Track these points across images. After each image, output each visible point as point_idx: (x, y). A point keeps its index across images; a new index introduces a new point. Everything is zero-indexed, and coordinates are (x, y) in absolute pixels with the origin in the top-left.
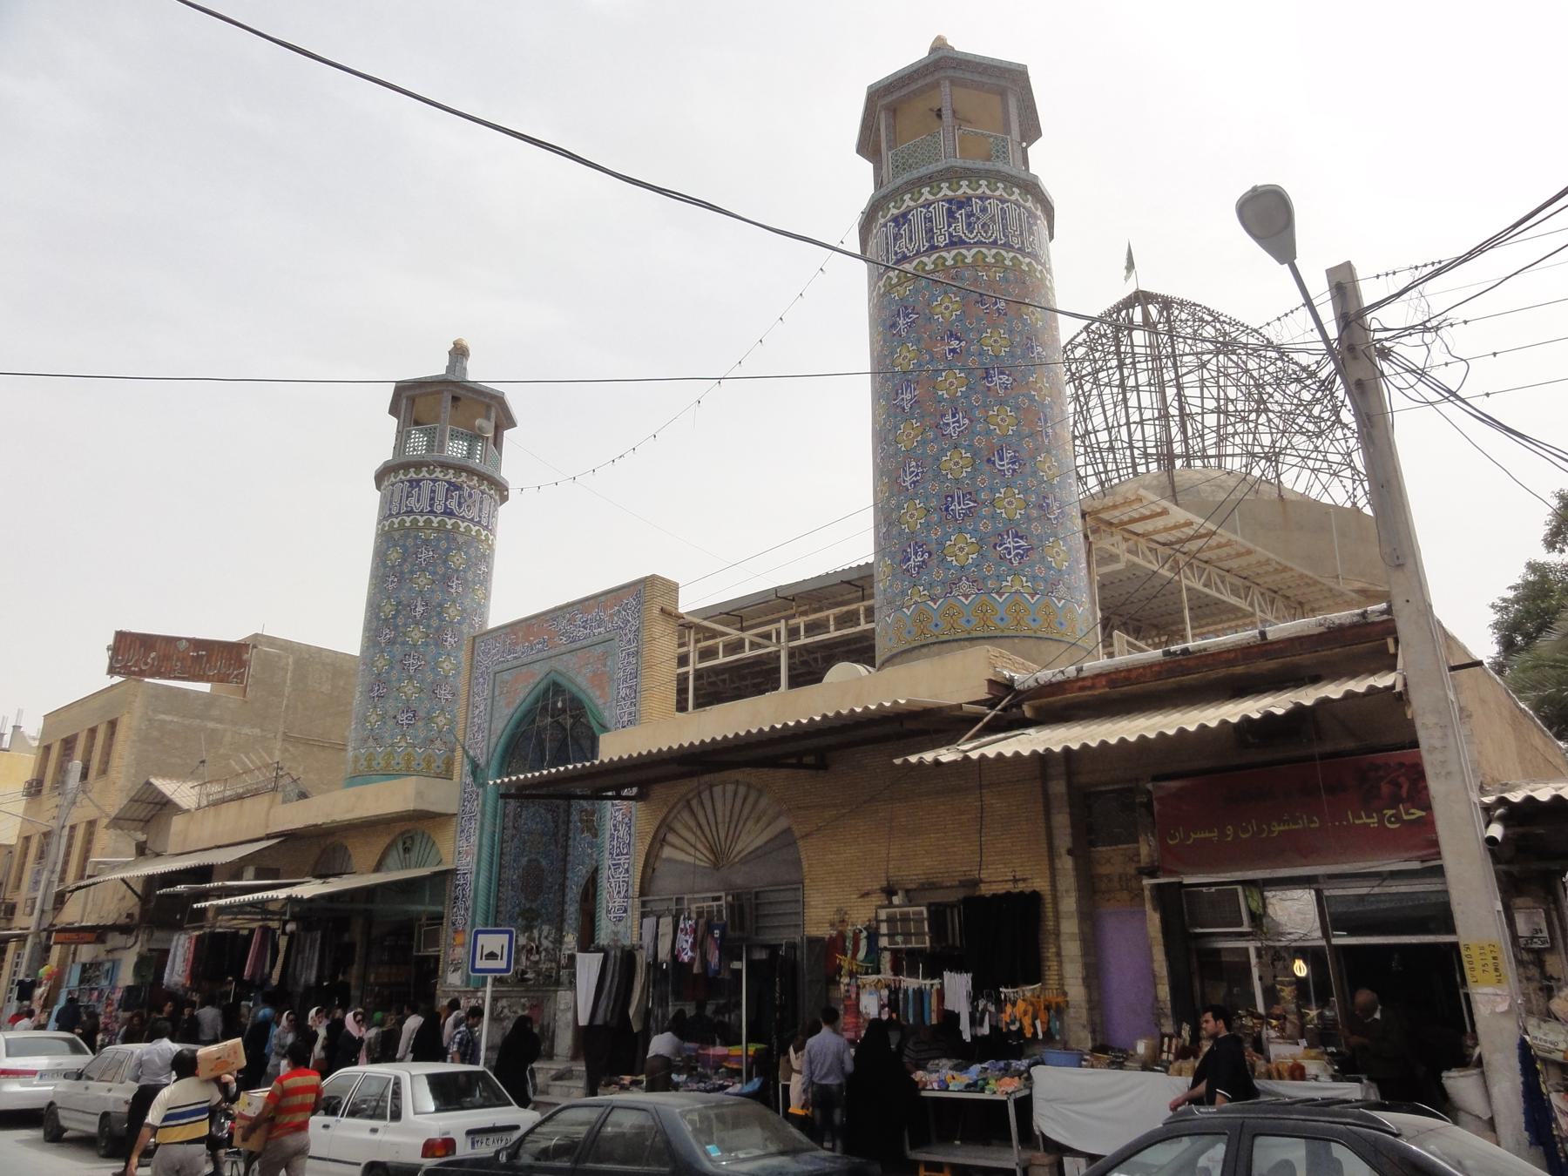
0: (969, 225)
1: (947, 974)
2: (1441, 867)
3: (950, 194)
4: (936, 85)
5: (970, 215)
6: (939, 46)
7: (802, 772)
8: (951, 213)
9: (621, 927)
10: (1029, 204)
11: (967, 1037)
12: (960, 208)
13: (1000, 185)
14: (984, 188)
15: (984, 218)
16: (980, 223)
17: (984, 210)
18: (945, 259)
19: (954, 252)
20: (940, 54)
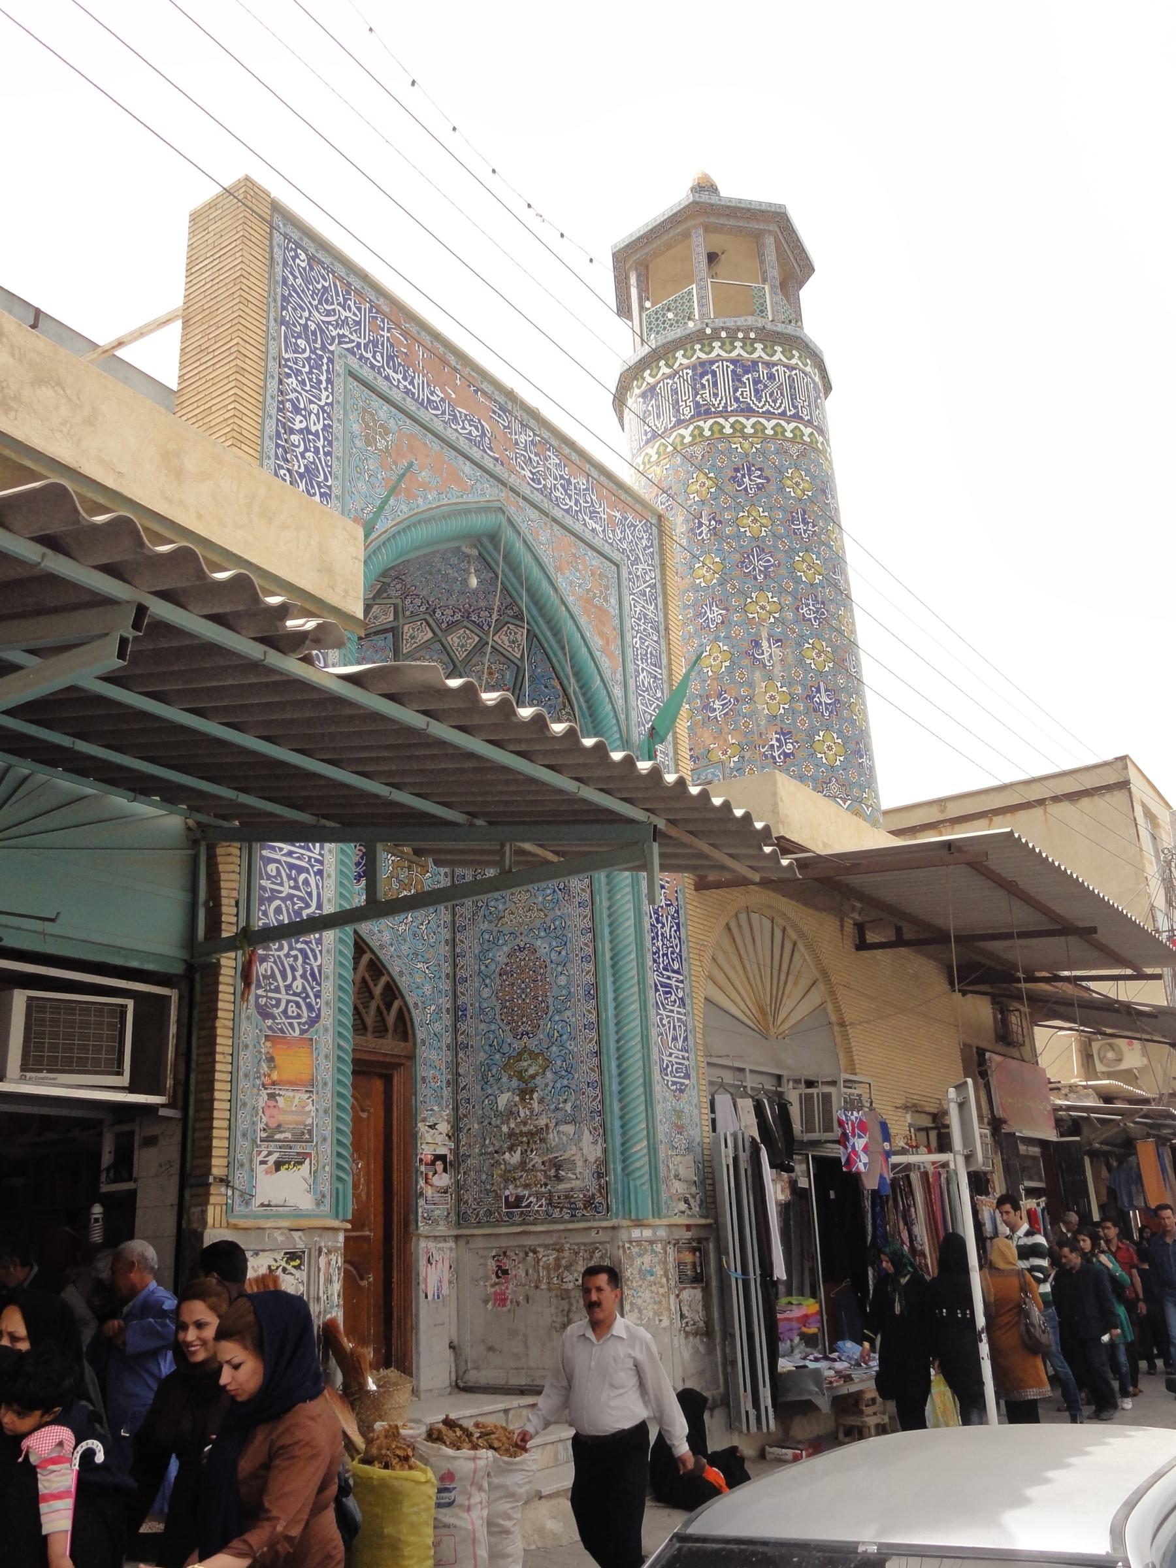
0: (757, 391)
1: (44, 1533)
2: (983, 1420)
3: (703, 356)
4: (687, 235)
5: (757, 382)
6: (705, 187)
7: (903, 951)
8: (737, 378)
9: (683, 1104)
10: (808, 369)
11: (879, 1337)
12: (746, 372)
13: (778, 349)
14: (759, 352)
15: (772, 386)
16: (768, 391)
17: (771, 377)
18: (683, 437)
19: (710, 422)
20: (704, 198)
